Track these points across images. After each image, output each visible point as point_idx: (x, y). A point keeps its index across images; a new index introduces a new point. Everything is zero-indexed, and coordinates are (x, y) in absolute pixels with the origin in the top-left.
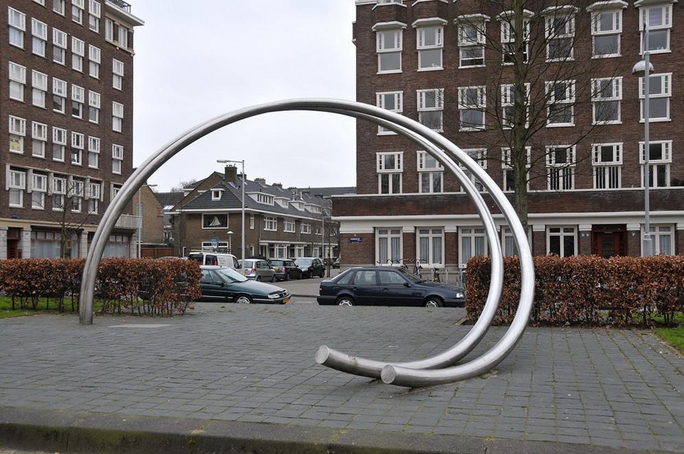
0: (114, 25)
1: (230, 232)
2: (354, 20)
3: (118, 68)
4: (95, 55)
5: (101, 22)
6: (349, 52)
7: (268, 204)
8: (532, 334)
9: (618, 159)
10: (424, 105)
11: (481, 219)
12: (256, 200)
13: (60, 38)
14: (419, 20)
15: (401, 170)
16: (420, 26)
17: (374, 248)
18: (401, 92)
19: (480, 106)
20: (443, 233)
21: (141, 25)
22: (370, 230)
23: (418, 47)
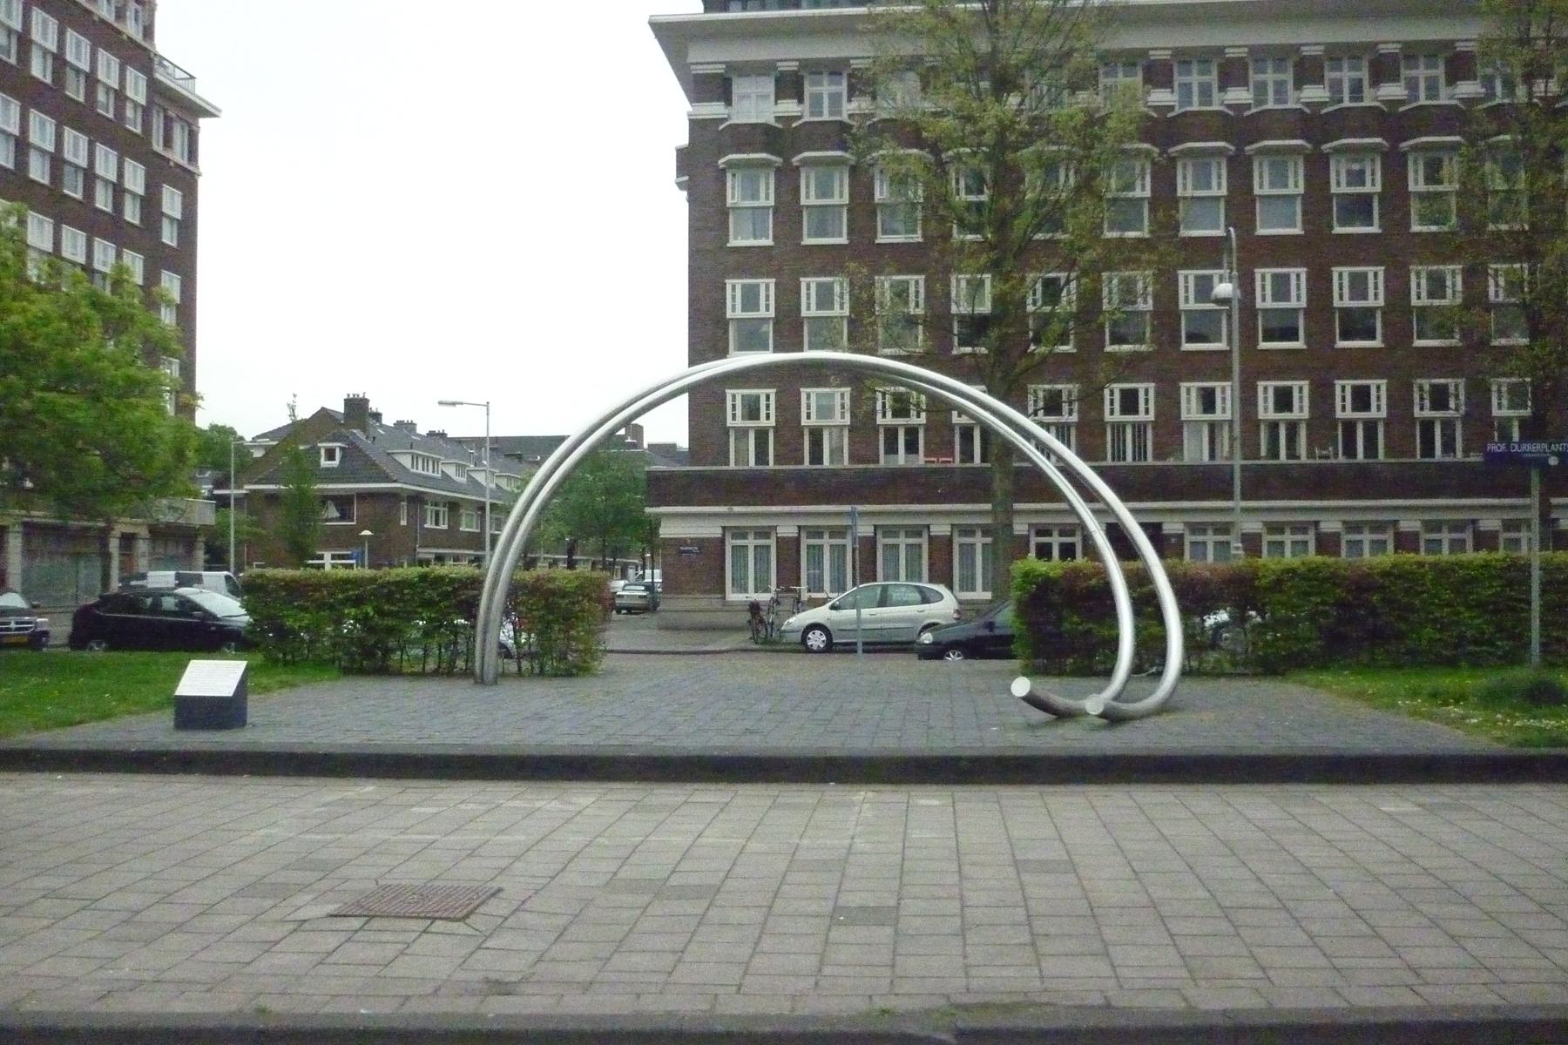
0: (166, 117)
1: (367, 533)
2: (683, 140)
3: (171, 202)
4: (135, 179)
5: (146, 111)
6: (676, 208)
7: (430, 473)
8: (1196, 687)
9: (1147, 412)
10: (813, 306)
11: (1072, 511)
12: (409, 466)
13: (76, 147)
14: (807, 154)
15: (772, 422)
16: (806, 163)
17: (723, 569)
18: (772, 281)
19: (912, 310)
20: (925, 535)
21: (214, 115)
22: (717, 532)
23: (803, 201)
